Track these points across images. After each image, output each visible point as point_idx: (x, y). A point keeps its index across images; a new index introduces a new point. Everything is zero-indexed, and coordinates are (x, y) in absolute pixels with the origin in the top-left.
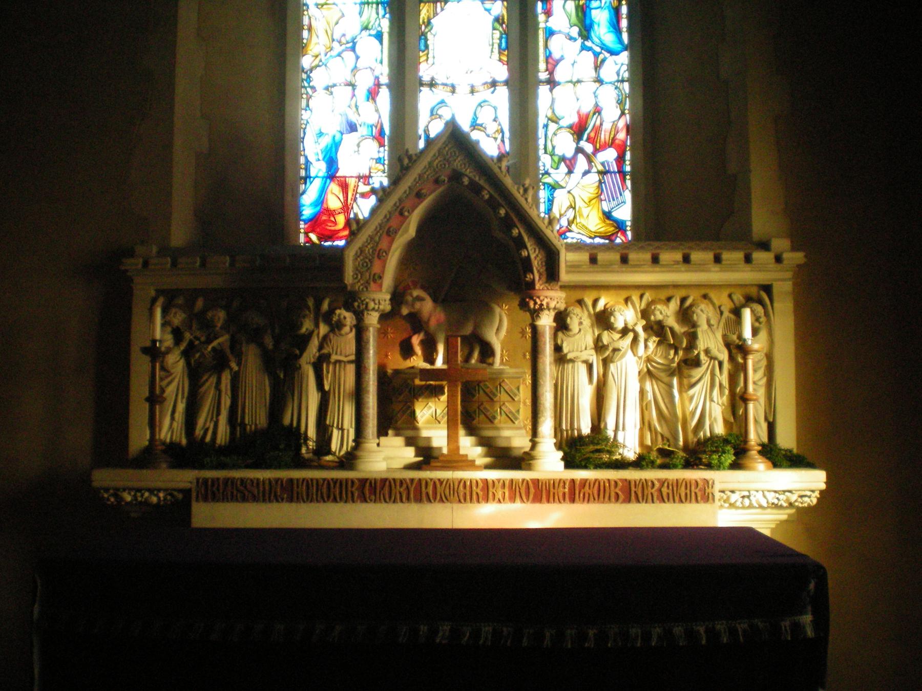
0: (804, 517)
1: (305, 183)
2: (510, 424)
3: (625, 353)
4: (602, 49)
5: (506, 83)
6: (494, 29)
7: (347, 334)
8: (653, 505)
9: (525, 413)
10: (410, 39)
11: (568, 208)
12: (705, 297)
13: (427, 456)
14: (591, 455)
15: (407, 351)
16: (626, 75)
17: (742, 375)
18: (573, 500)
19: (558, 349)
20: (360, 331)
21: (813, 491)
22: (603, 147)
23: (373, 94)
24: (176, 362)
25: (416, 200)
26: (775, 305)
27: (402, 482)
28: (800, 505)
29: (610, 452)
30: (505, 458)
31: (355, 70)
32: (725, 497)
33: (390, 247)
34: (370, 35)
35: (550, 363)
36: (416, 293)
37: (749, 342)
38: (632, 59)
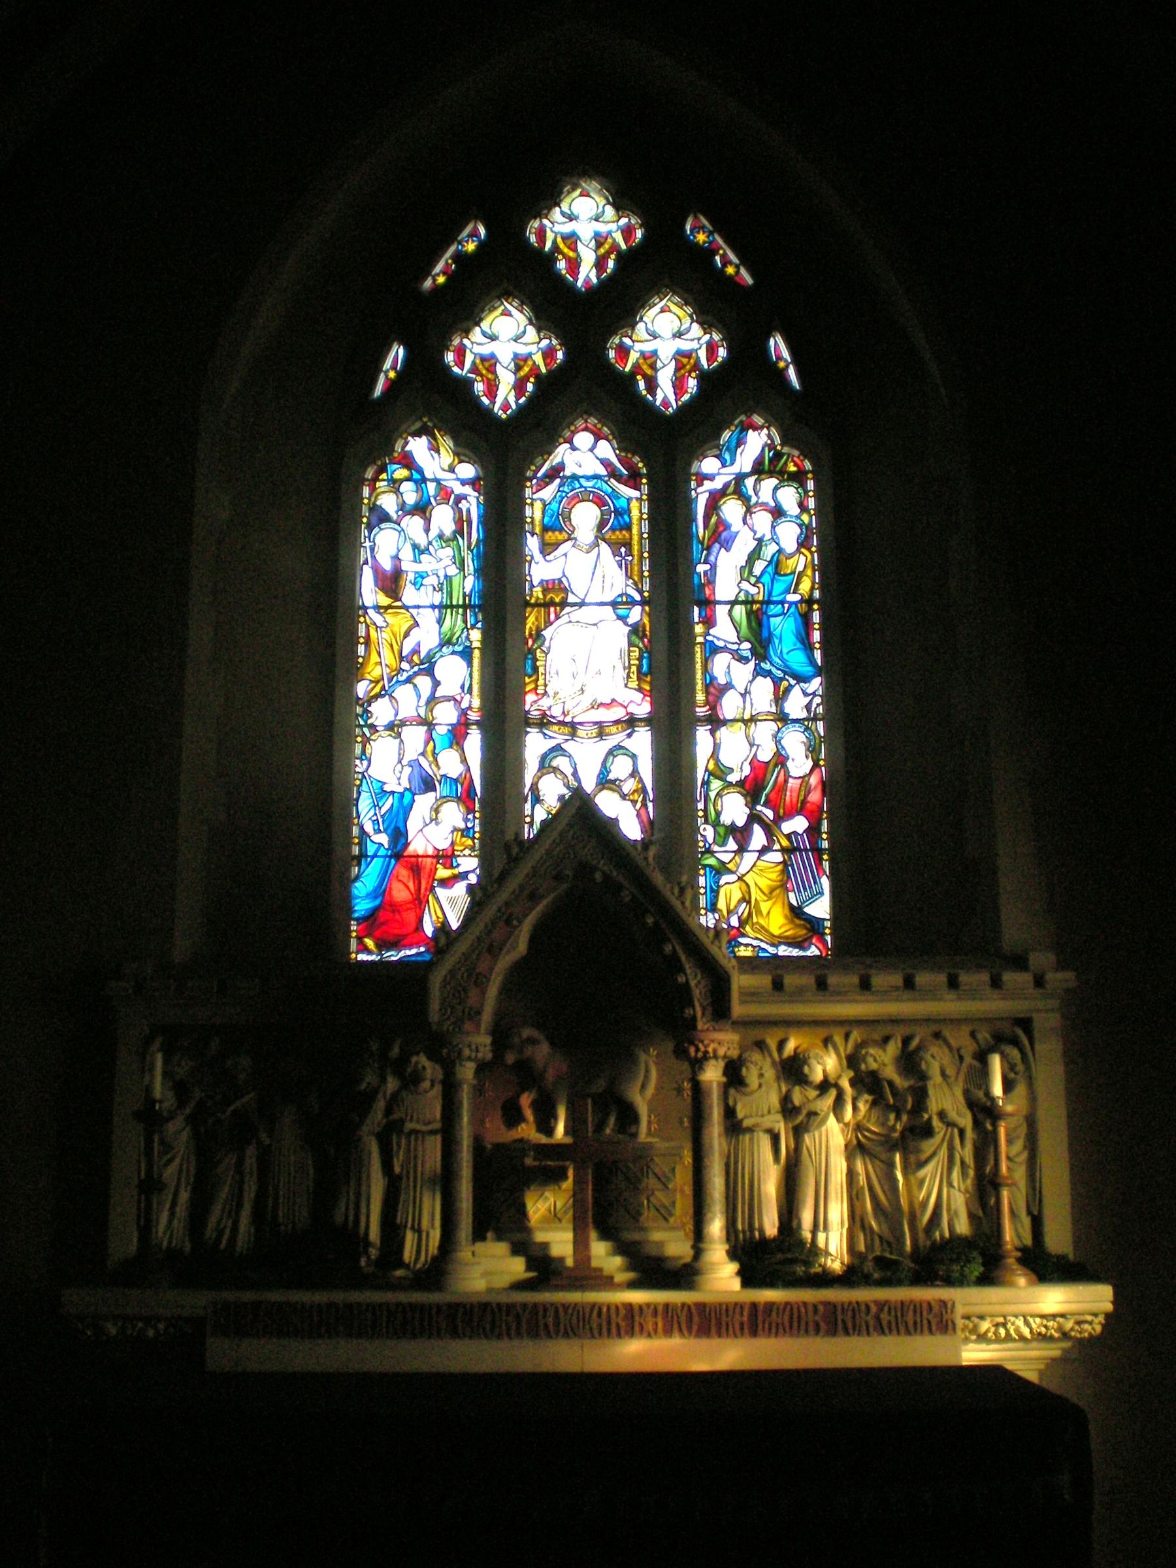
0: (1083, 1352)
1: (359, 865)
2: (662, 1223)
3: (824, 1121)
4: (785, 673)
5: (648, 721)
6: (630, 644)
7: (426, 1092)
8: (867, 1339)
9: (683, 1206)
10: (511, 660)
11: (740, 902)
12: (937, 1035)
13: (544, 1268)
14: (777, 1267)
15: (513, 1116)
16: (820, 710)
17: (992, 1149)
18: (754, 1333)
19: (729, 1113)
20: (450, 1088)
21: (1095, 1315)
22: (789, 815)
23: (458, 735)
24: (178, 1131)
25: (529, 904)
26: (1038, 1047)
27: (510, 1307)
28: (1078, 1335)
29: (808, 1263)
30: (653, 1271)
31: (433, 700)
32: (971, 1325)
33: (491, 969)
34: (453, 653)
35: (720, 1135)
36: (526, 1032)
37: (1001, 1103)
38: (828, 687)
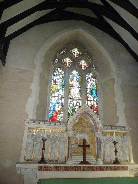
18: (106, 170)
31: (59, 94)
